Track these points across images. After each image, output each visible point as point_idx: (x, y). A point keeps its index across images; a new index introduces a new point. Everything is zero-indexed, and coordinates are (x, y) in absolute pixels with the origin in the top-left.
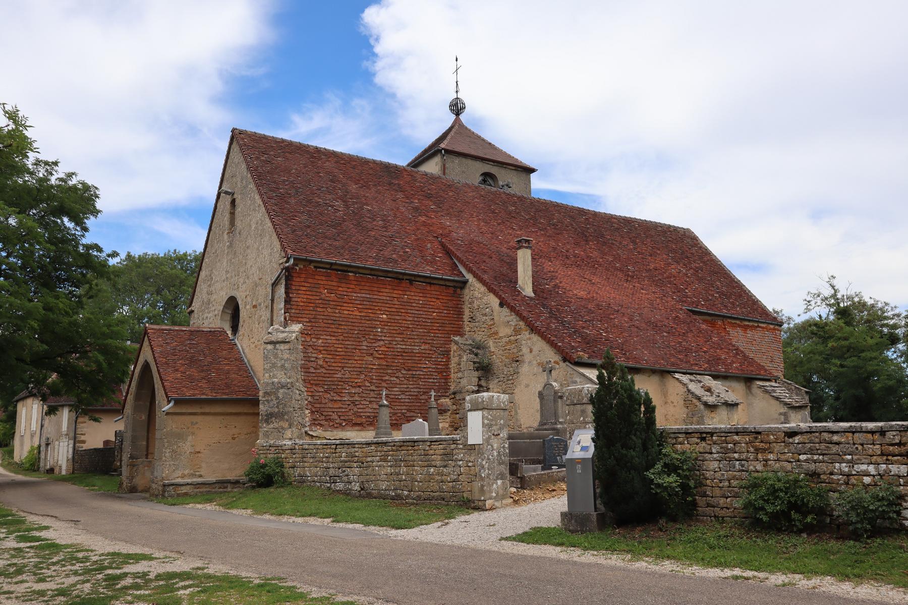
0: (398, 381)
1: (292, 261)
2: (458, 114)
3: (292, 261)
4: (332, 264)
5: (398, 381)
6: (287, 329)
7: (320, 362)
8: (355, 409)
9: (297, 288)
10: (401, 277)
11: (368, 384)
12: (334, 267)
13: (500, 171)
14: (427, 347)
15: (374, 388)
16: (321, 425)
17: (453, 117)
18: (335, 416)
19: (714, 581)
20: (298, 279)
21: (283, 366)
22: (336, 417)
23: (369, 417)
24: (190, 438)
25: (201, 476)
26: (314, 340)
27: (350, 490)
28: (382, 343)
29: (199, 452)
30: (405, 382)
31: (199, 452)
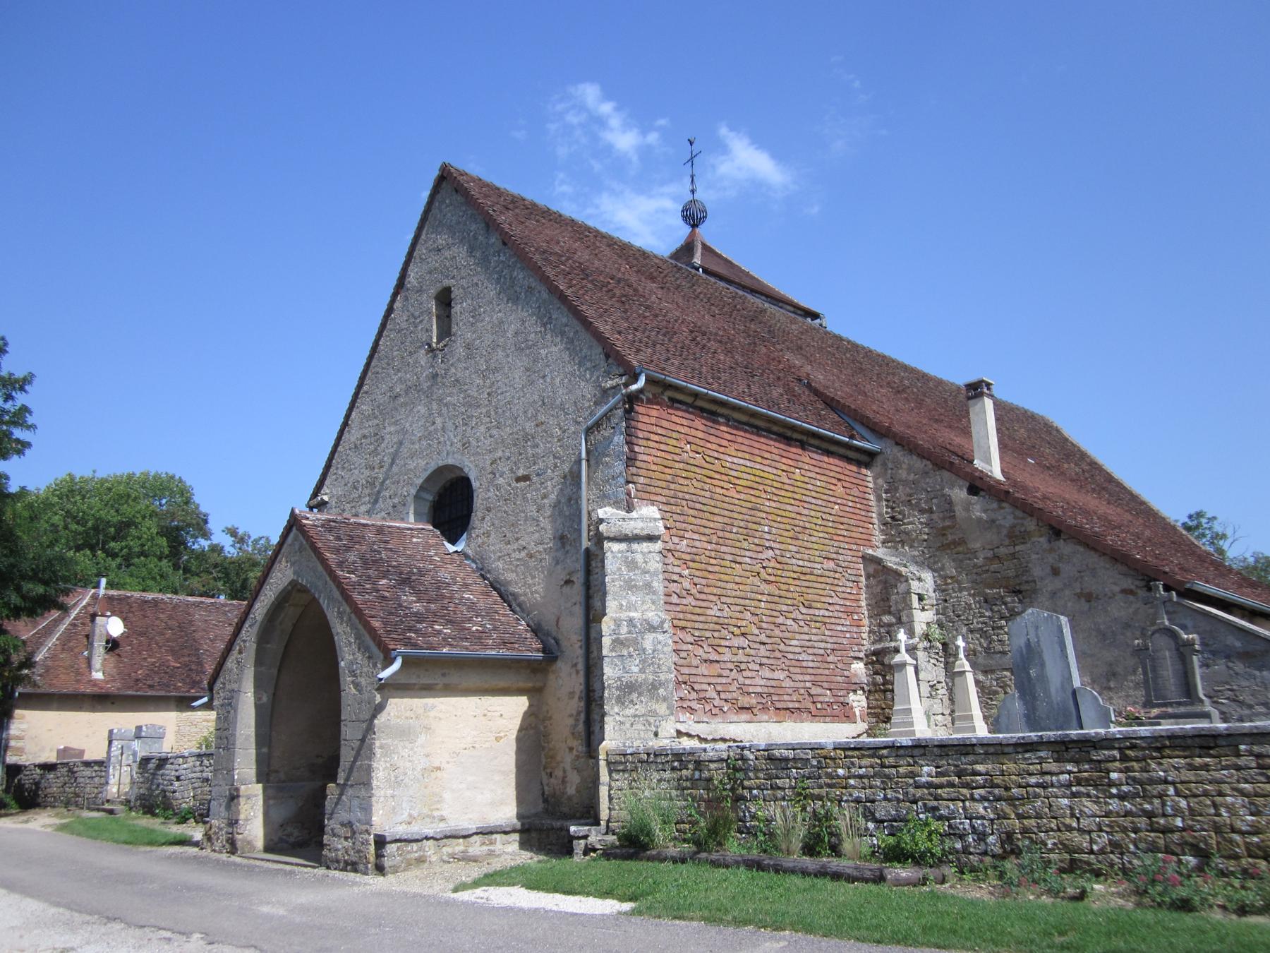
0: (796, 627)
1: (641, 382)
2: (694, 226)
3: (641, 382)
4: (696, 395)
5: (796, 627)
6: (634, 514)
7: (687, 584)
8: (741, 680)
9: (646, 435)
10: (789, 433)
11: (757, 632)
12: (699, 403)
13: (206, 522)
14: (831, 564)
15: (764, 639)
16: (692, 710)
17: (688, 230)
18: (711, 693)
19: (603, 917)
20: (645, 419)
21: (648, 586)
22: (714, 695)
23: (760, 694)
24: (422, 739)
25: (443, 819)
26: (676, 540)
27: (729, 829)
28: (770, 553)
29: (439, 769)
30: (806, 629)
31: (439, 769)
